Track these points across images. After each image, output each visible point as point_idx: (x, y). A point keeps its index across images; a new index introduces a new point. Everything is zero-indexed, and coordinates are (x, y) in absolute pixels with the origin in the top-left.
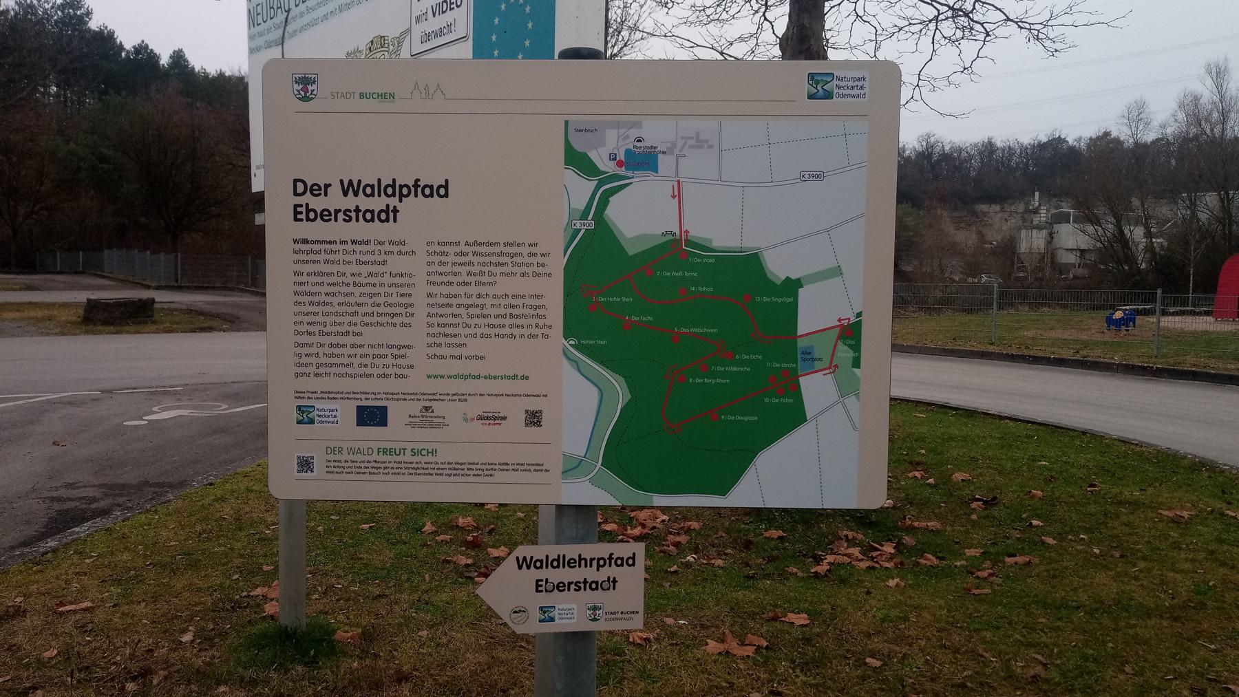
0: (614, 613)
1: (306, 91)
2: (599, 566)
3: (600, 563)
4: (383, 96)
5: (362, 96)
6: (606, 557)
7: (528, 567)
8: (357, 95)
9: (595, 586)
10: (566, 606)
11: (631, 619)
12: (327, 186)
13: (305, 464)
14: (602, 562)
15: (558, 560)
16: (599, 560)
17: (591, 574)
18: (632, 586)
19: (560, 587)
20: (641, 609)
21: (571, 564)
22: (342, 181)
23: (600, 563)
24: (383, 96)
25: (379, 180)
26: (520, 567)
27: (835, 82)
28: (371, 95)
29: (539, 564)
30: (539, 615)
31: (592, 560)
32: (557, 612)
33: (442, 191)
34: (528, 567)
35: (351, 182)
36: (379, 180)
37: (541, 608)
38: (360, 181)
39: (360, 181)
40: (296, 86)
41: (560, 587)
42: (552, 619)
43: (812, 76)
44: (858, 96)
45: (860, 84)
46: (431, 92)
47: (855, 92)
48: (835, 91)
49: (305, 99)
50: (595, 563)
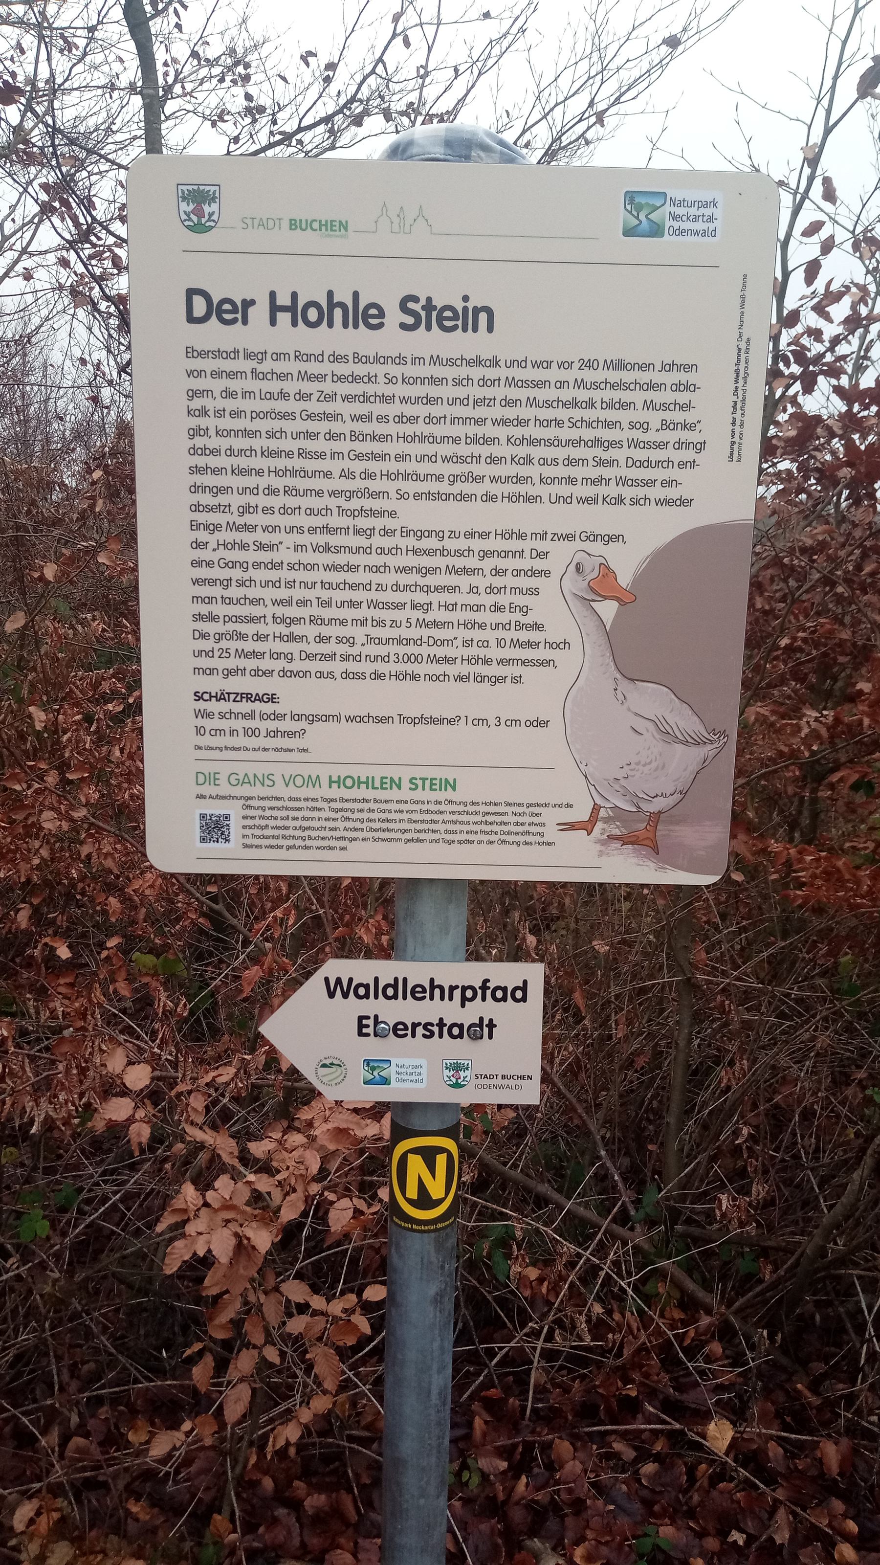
0: (491, 1077)
1: (199, 213)
2: (464, 1000)
3: (468, 995)
5: (294, 224)
6: (477, 984)
7: (345, 995)
8: (285, 224)
9: (457, 1031)
10: (407, 1062)
11: (519, 1087)
12: (248, 304)
13: (214, 828)
14: (469, 994)
15: (395, 986)
16: (464, 989)
17: (451, 1011)
18: (521, 1031)
19: (399, 1030)
20: (537, 1076)
21: (417, 993)
23: (468, 995)
26: (331, 995)
27: (668, 208)
28: (310, 225)
29: (363, 991)
30: (364, 1074)
31: (452, 989)
32: (393, 1068)
34: (345, 995)
35: (339, 981)
37: (367, 1062)
38: (351, 980)
39: (351, 980)
40: (184, 206)
41: (399, 1030)
42: (385, 1081)
44: (704, 234)
45: (708, 212)
46: (409, 221)
47: (699, 226)
49: (199, 228)
50: (457, 993)
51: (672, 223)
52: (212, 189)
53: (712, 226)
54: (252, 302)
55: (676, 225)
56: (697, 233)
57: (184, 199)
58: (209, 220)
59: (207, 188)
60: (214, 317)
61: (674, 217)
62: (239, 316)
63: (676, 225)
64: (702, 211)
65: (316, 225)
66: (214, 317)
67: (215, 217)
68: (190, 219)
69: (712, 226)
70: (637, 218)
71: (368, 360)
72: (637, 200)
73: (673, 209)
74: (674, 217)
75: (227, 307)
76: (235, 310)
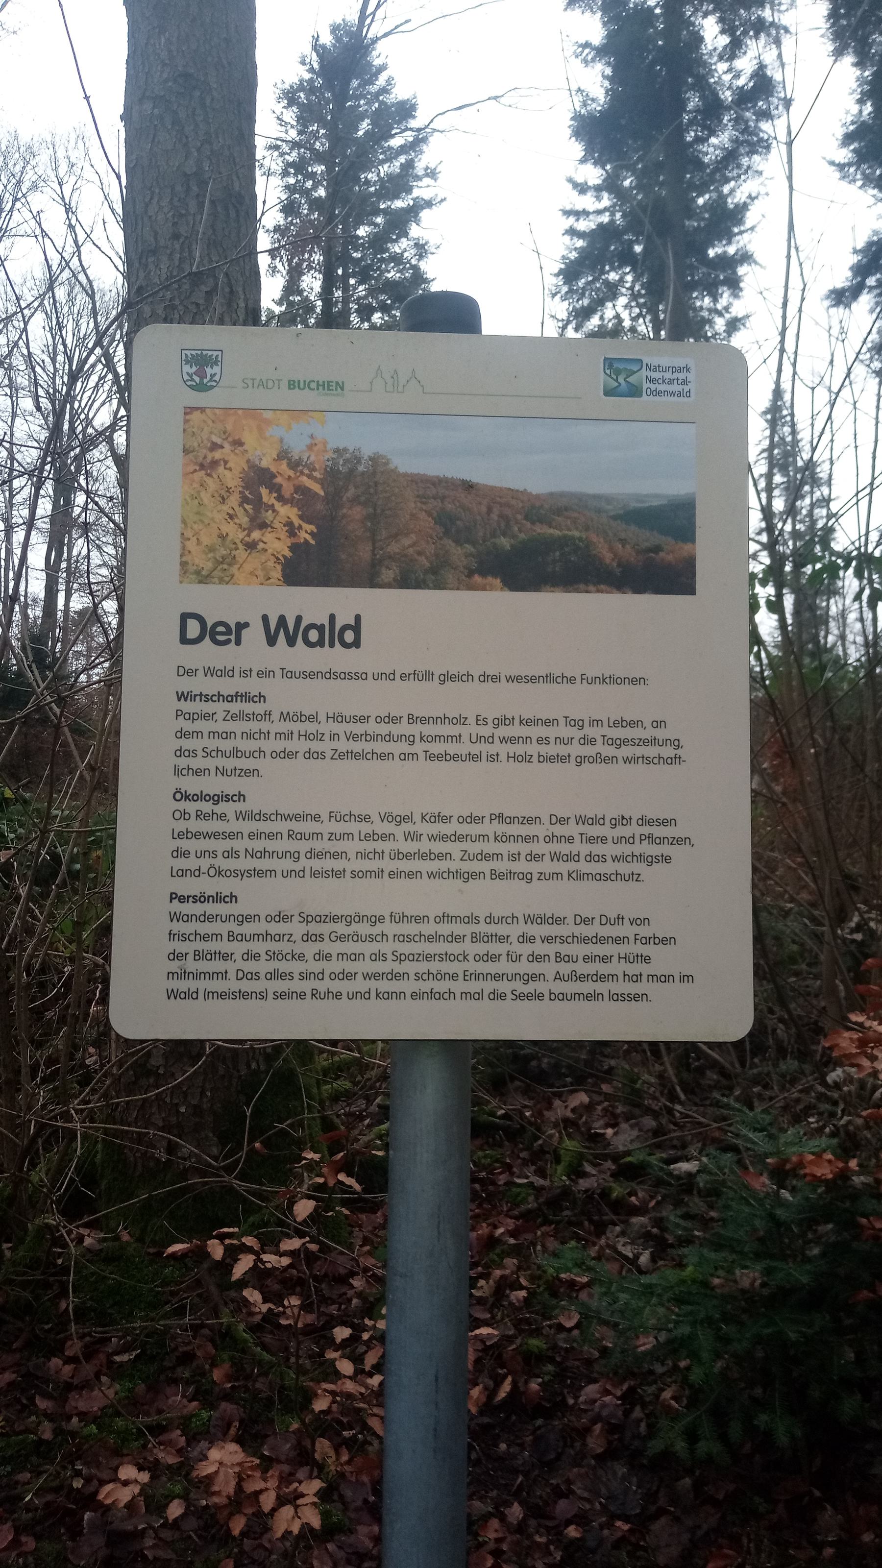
1: (202, 376)
4: (326, 386)
8: (284, 384)
12: (242, 626)
22: (265, 618)
24: (326, 386)
25: (332, 618)
27: (644, 373)
28: (308, 385)
33: (349, 636)
34: (291, 642)
35: (282, 620)
36: (332, 618)
38: (299, 619)
39: (299, 619)
40: (187, 368)
43: (609, 363)
44: (680, 394)
45: (682, 376)
47: (675, 388)
48: (645, 387)
49: (201, 388)
51: (649, 385)
52: (215, 353)
53: (686, 388)
54: (247, 625)
55: (653, 387)
56: (672, 394)
57: (187, 362)
58: (211, 380)
59: (210, 353)
60: (207, 637)
61: (651, 381)
62: (233, 637)
63: (653, 387)
64: (676, 375)
65: (313, 385)
66: (207, 637)
67: (217, 378)
68: (193, 380)
69: (686, 388)
70: (617, 380)
71: (342, 818)
72: (615, 366)
73: (649, 374)
74: (651, 381)
75: (221, 629)
76: (229, 631)
